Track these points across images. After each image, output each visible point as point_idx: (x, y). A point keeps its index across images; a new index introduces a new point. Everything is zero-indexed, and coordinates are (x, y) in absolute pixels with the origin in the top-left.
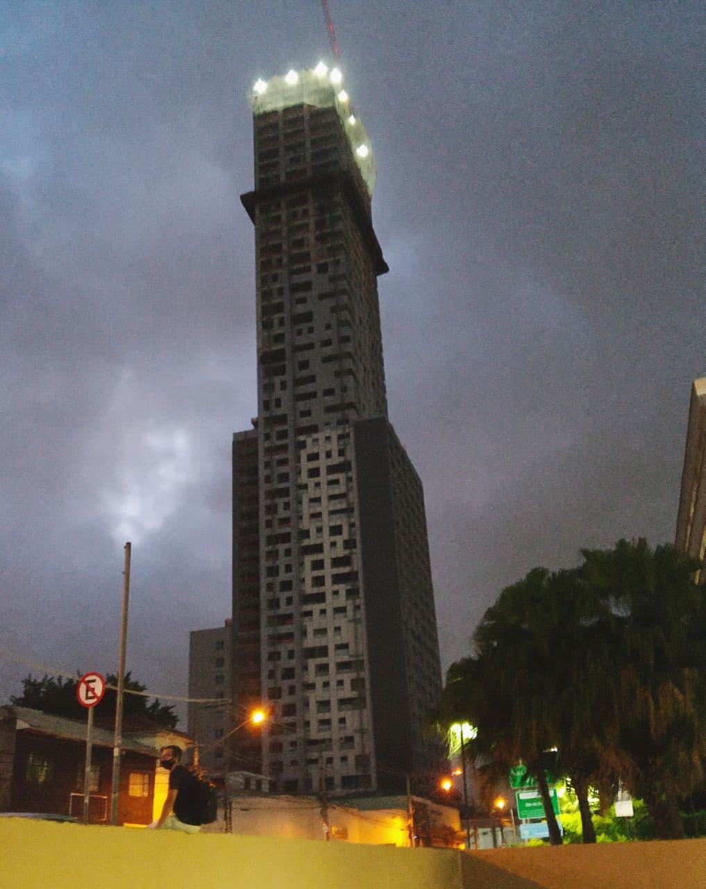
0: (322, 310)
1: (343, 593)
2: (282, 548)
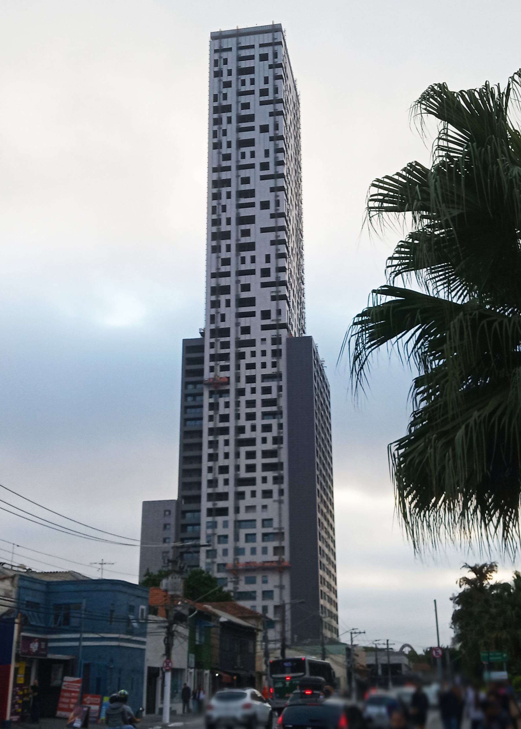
1: (270, 480)
2: (221, 439)
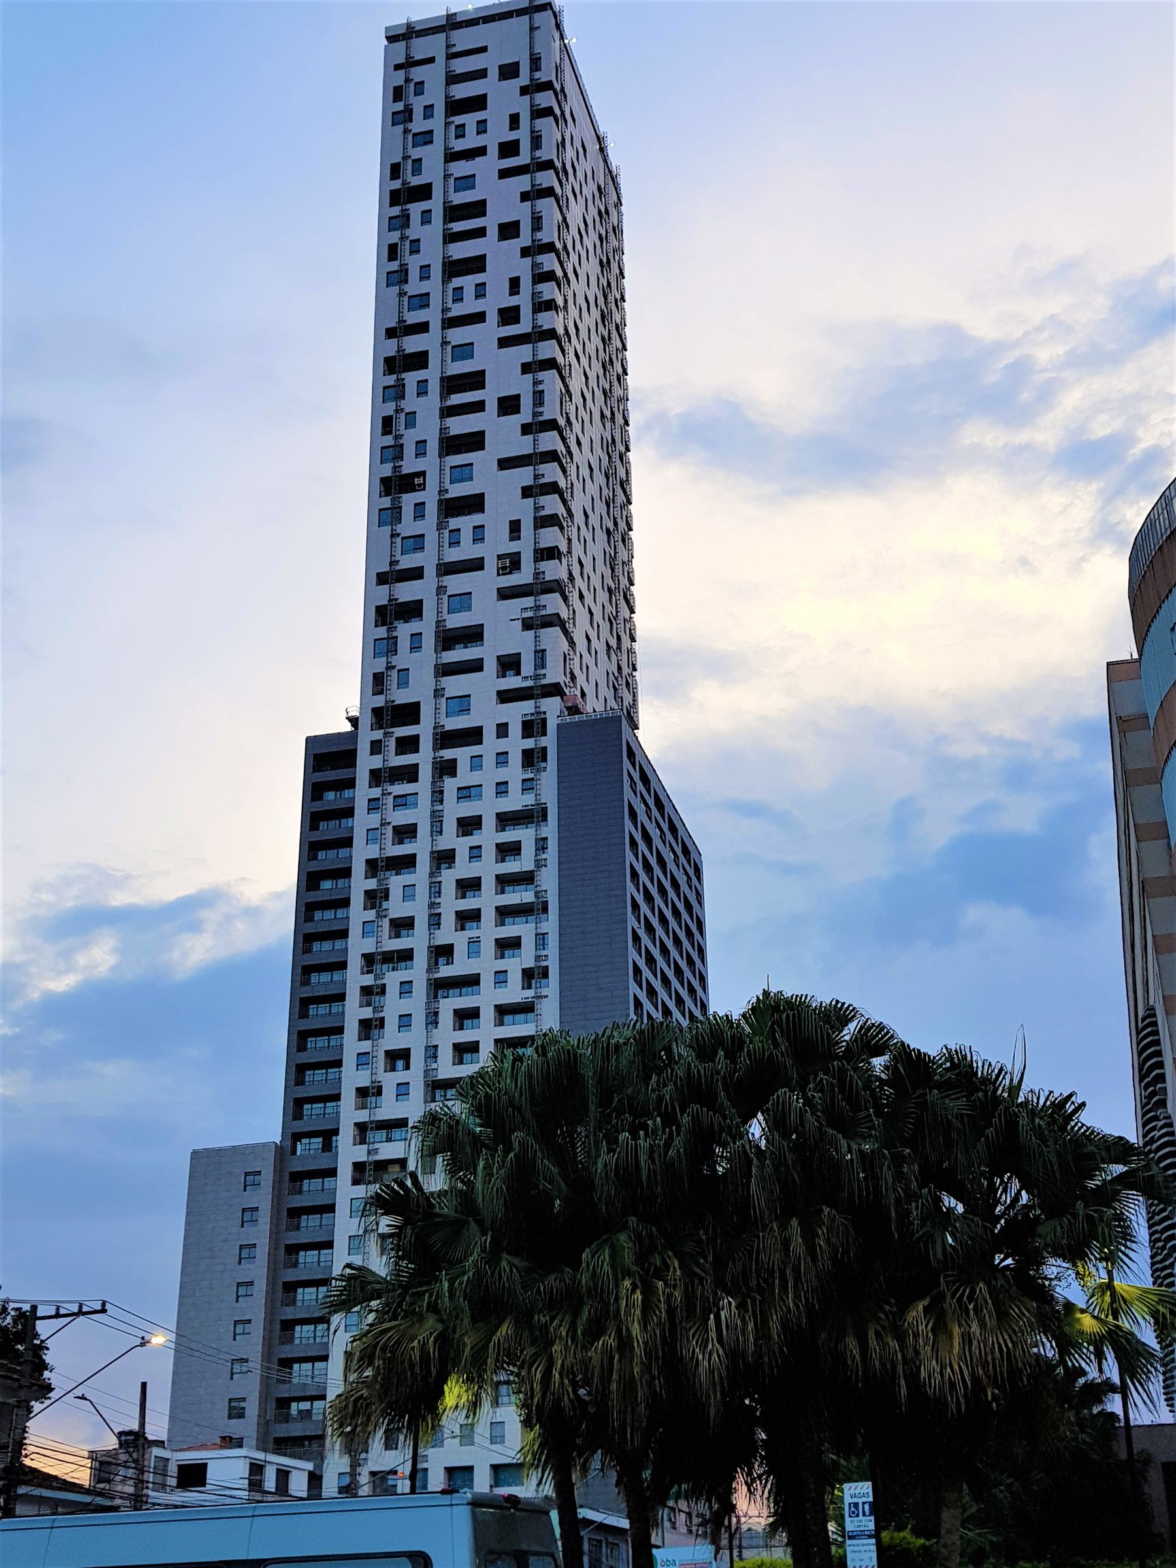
0: (505, 496)
